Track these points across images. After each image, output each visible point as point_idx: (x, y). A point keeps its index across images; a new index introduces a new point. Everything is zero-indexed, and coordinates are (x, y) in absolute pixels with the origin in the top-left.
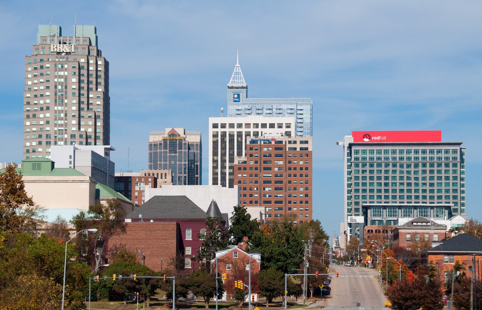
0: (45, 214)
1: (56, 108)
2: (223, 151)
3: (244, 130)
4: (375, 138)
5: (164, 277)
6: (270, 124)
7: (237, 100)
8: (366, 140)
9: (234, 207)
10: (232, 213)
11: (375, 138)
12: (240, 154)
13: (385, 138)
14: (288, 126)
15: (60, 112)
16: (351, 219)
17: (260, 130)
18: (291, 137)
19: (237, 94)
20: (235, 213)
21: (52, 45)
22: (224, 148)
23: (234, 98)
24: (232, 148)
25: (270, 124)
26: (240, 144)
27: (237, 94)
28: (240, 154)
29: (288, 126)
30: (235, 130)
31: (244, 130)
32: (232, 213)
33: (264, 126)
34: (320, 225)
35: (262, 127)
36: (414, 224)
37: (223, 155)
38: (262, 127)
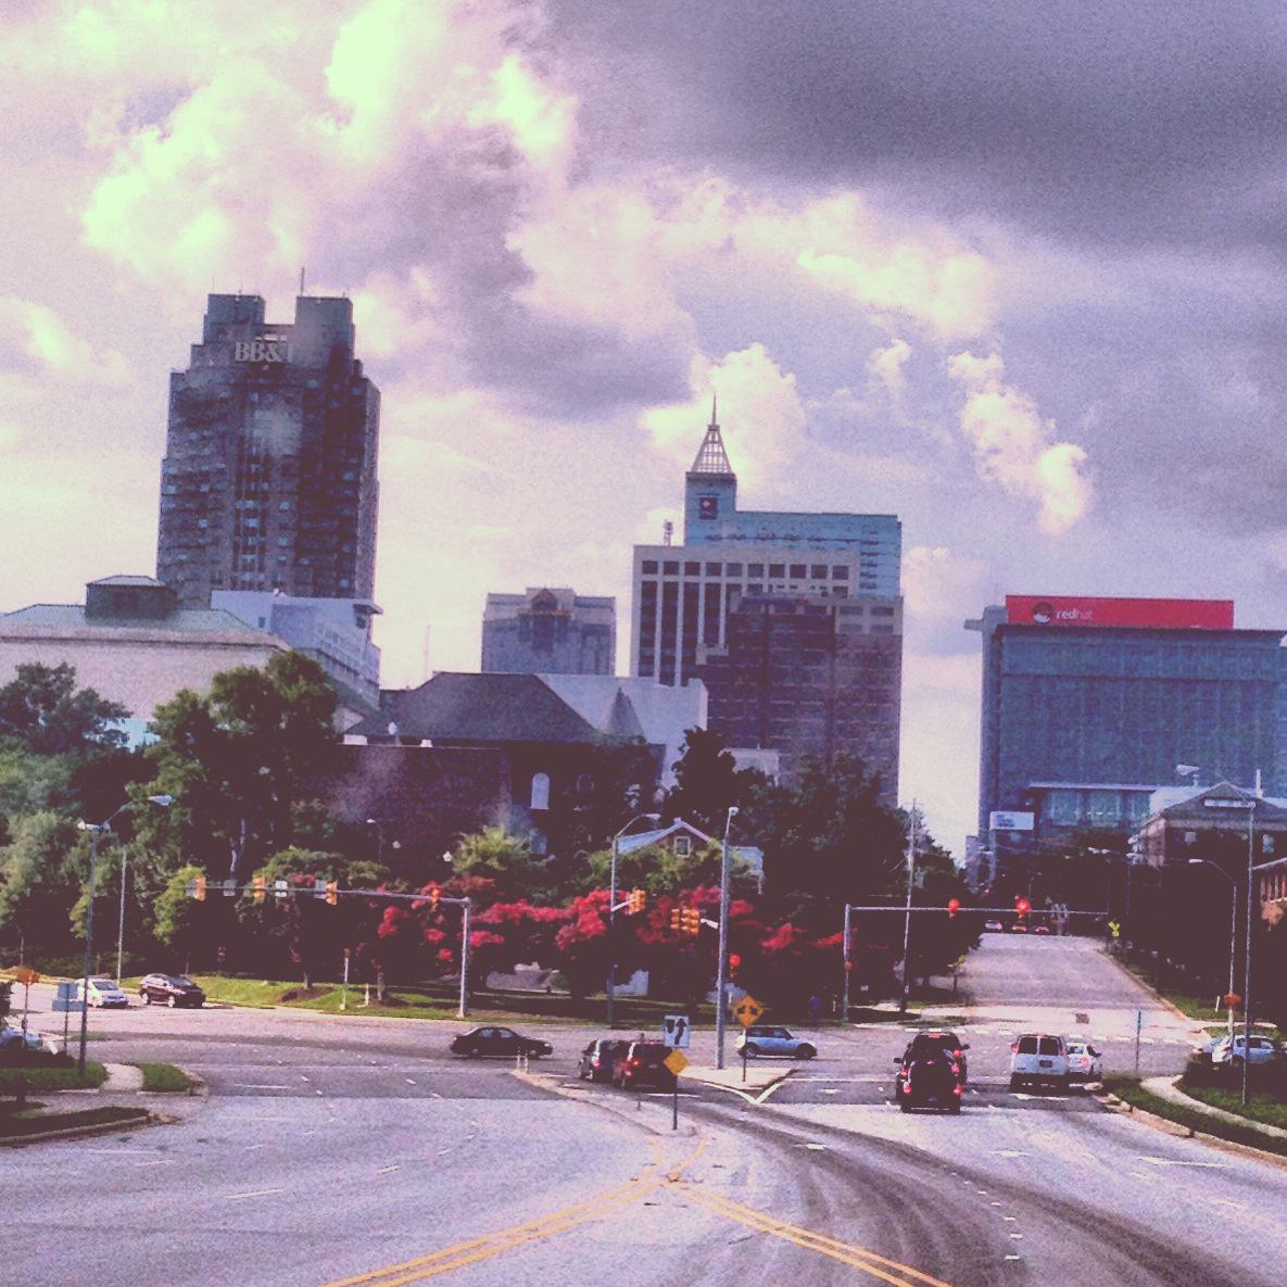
0: (122, 728)
1: (239, 505)
2: (668, 652)
3: (724, 580)
4: (1065, 615)
5: (434, 900)
6: (793, 567)
7: (709, 514)
8: (1041, 618)
9: (686, 731)
10: (681, 749)
11: (1065, 615)
12: (711, 640)
13: (1089, 615)
14: (841, 573)
15: (251, 513)
16: (1002, 822)
17: (765, 581)
18: (846, 597)
19: (708, 500)
20: (687, 748)
21: (238, 344)
22: (669, 625)
23: (703, 508)
24: (690, 628)
25: (793, 567)
26: (712, 613)
27: (708, 500)
28: (711, 640)
29: (841, 573)
30: (703, 579)
31: (724, 580)
32: (681, 749)
33: (777, 570)
34: (923, 823)
35: (771, 575)
36: (1208, 803)
37: (669, 643)
38: (771, 575)
